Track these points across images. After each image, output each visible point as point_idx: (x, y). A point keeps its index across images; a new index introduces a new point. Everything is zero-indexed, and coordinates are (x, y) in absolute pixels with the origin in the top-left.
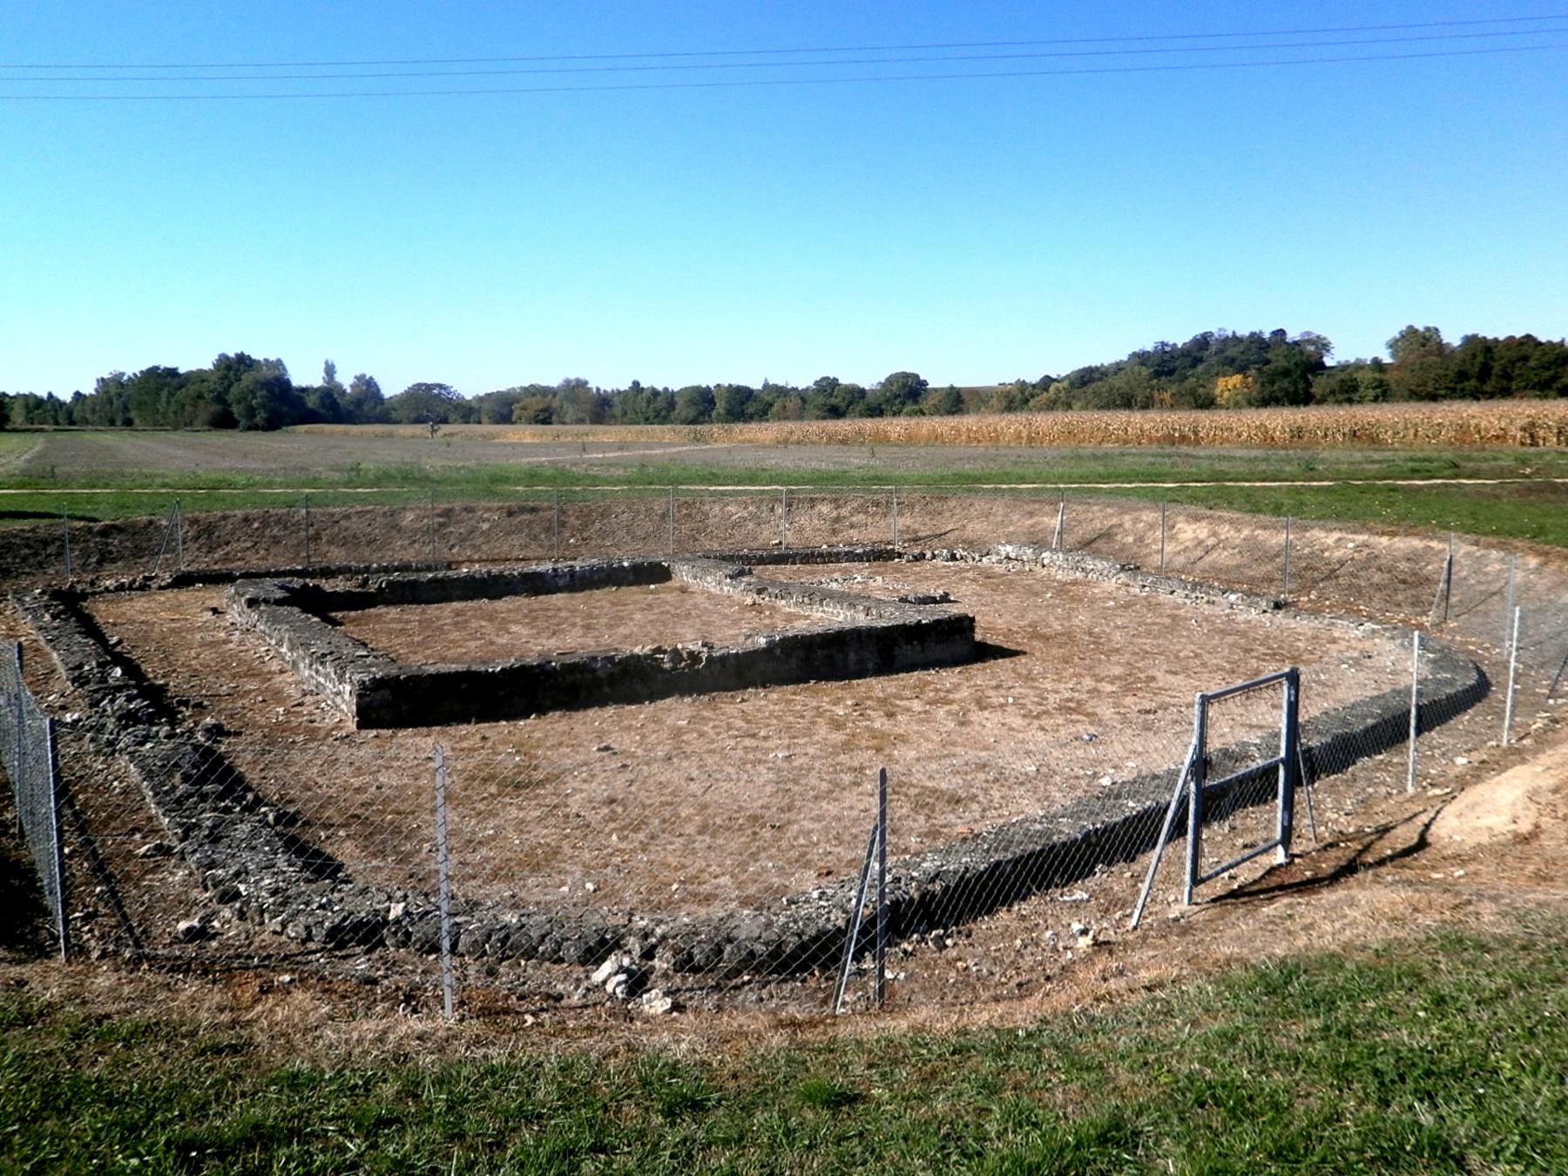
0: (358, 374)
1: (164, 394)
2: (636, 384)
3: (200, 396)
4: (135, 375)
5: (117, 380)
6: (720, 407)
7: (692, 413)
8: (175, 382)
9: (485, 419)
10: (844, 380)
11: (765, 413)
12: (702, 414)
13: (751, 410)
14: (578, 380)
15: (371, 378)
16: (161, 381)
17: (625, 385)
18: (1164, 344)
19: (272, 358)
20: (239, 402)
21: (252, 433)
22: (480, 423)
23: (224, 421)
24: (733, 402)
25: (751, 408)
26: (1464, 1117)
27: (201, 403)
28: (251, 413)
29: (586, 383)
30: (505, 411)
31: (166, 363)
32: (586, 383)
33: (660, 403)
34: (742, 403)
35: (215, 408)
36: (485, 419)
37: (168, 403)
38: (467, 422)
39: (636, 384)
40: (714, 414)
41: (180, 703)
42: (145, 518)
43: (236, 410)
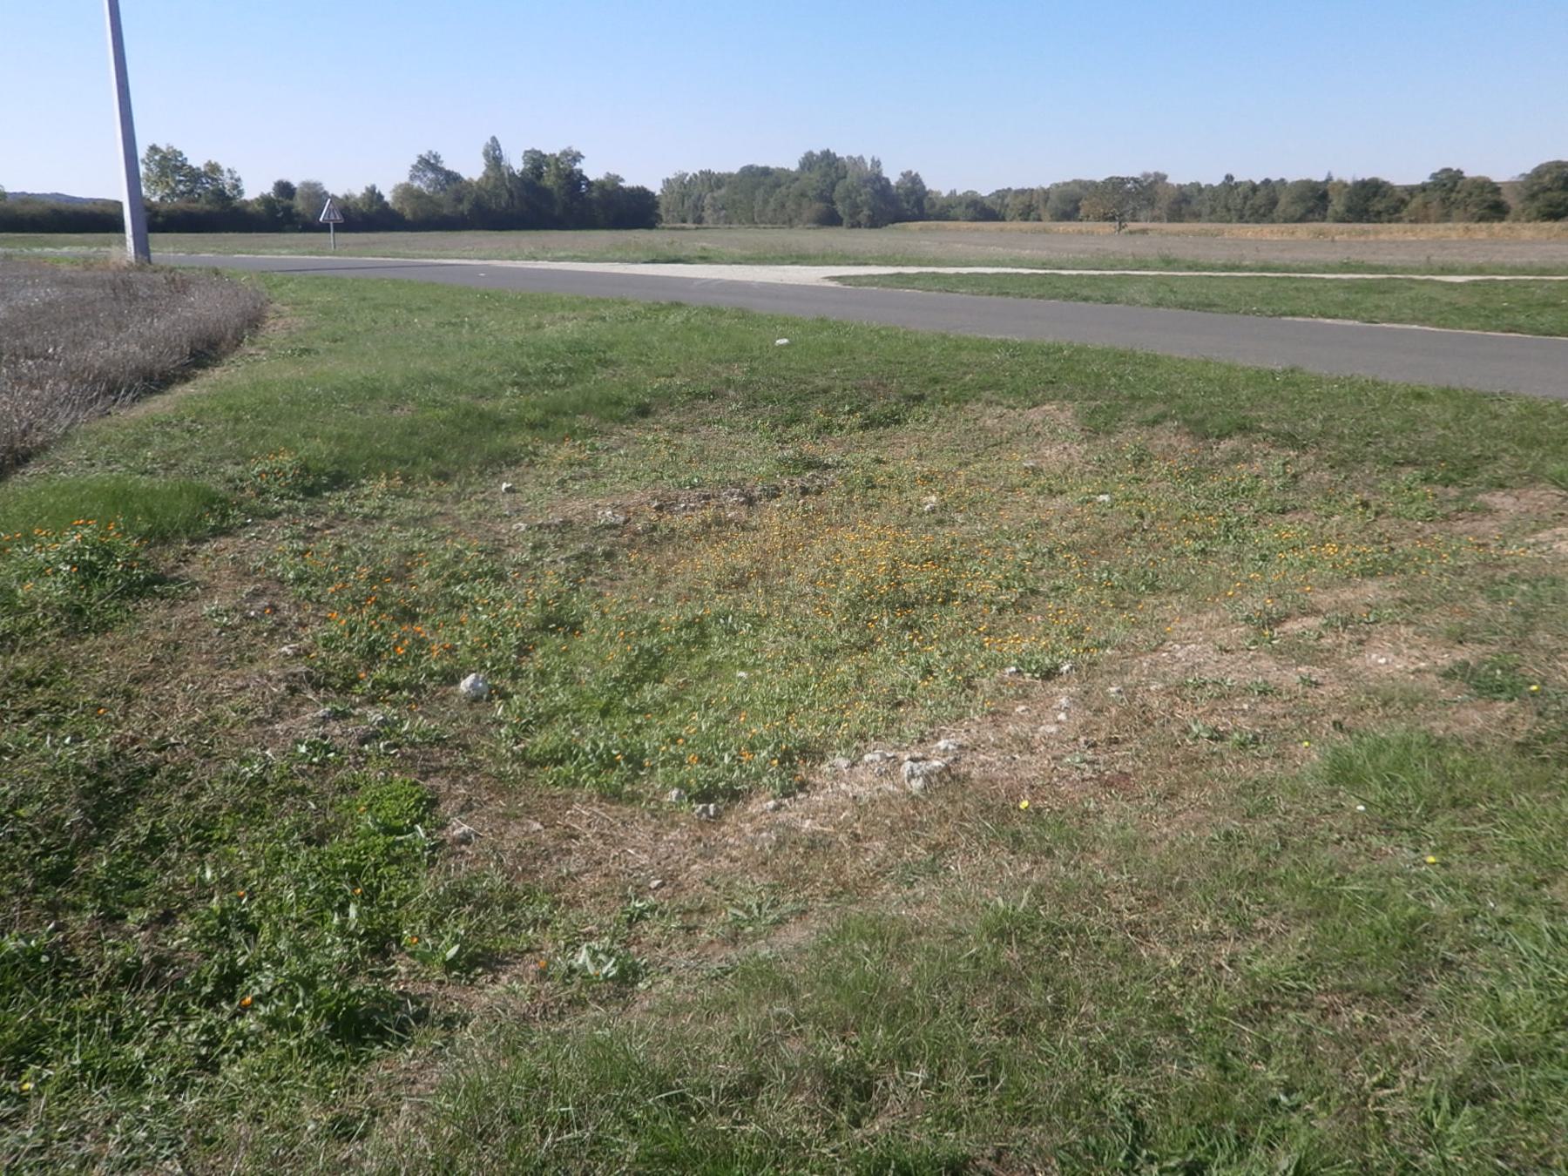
0: (905, 171)
1: (760, 194)
2: (1229, 178)
3: (803, 195)
4: (695, 175)
5: (680, 179)
6: (1337, 204)
7: (1299, 210)
8: (769, 181)
9: (1046, 215)
10: (1470, 173)
11: (1397, 210)
12: (1311, 211)
13: (1381, 207)
14: (1157, 174)
15: (917, 175)
16: (758, 179)
17: (1217, 180)
18: (617, 178)
19: (855, 156)
20: (843, 200)
21: (856, 231)
22: (1039, 220)
23: (830, 219)
24: (1355, 198)
25: (1378, 205)
26: (129, 697)
27: (805, 202)
28: (855, 209)
29: (1165, 177)
30: (1069, 208)
31: (761, 163)
32: (1165, 177)
33: (1260, 198)
34: (1368, 200)
35: (819, 206)
36: (1046, 215)
37: (766, 202)
38: (1026, 220)
39: (1229, 178)
40: (1330, 211)
41: (495, 977)
42: (1449, 489)
43: (840, 208)
